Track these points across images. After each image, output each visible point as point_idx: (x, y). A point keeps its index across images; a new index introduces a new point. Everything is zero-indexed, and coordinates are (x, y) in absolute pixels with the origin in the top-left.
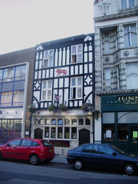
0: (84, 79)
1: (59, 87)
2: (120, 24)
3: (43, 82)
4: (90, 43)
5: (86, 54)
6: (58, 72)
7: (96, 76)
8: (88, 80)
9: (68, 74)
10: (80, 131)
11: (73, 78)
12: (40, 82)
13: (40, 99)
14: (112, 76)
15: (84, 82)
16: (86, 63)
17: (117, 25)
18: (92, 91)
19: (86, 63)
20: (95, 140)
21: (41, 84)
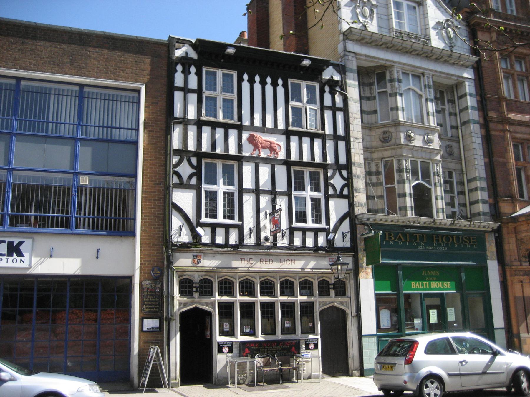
0: (326, 179)
1: (270, 189)
2: (397, 65)
3: (204, 161)
4: (338, 89)
5: (328, 115)
6: (251, 140)
7: (355, 176)
8: (338, 182)
9: (282, 155)
10: (321, 312)
11: (209, 161)
12: (194, 160)
13: (199, 216)
14: (370, 180)
15: (327, 185)
16: (101, 127)
17: (393, 64)
18: (347, 210)
19: (101, 127)
20: (364, 333)
21: (198, 168)
